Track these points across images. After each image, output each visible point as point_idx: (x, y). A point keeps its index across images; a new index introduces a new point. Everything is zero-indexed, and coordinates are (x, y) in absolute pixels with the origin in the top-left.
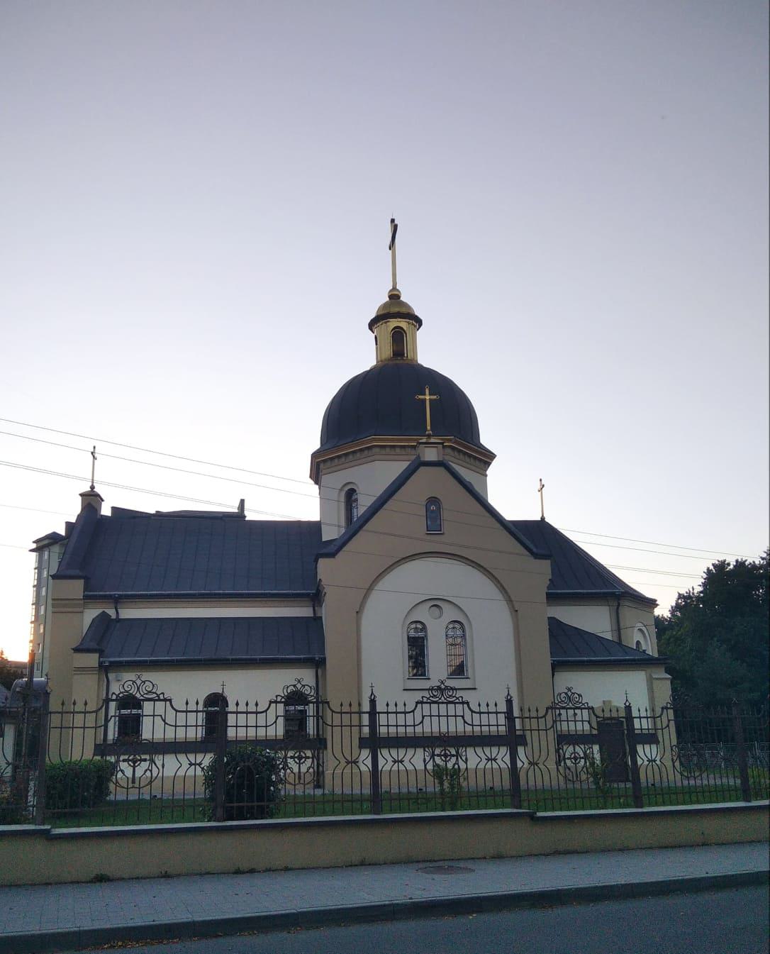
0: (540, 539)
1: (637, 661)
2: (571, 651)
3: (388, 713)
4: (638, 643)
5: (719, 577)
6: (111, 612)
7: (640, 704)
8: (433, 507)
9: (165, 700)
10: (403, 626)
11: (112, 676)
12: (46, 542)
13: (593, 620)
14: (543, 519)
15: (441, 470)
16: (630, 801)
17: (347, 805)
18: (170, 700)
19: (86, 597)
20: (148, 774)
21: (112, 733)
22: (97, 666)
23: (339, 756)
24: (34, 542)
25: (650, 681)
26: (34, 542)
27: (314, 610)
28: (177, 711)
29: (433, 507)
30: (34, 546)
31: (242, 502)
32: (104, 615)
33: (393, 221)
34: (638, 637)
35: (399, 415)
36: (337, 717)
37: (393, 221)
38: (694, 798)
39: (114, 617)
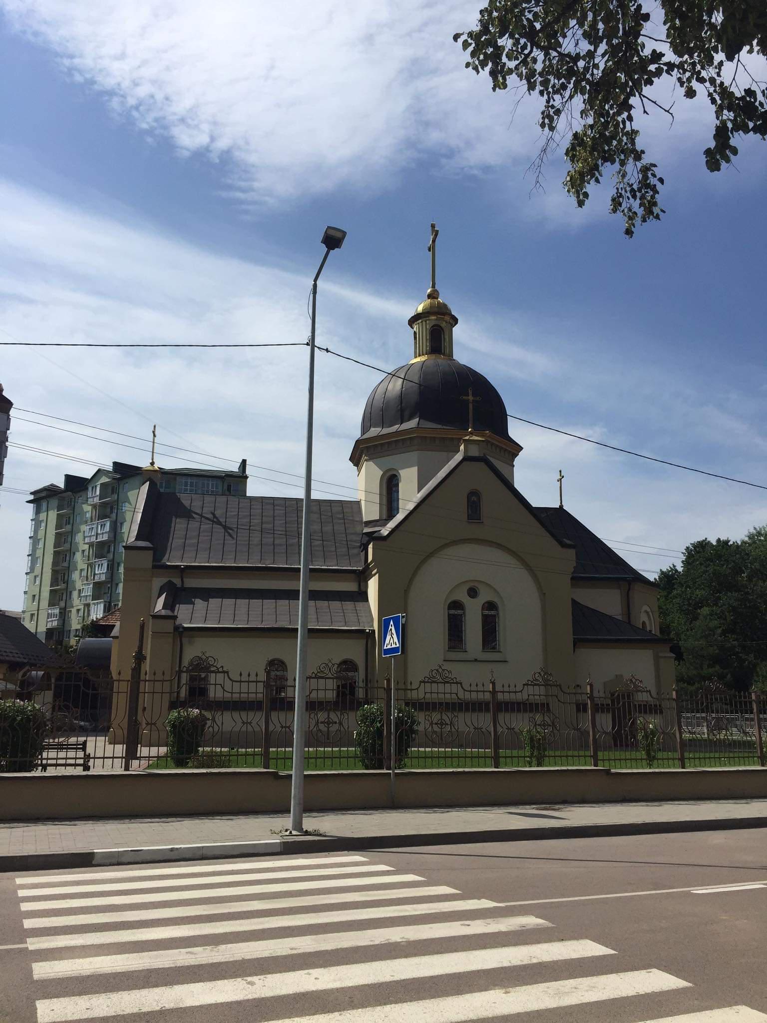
0: (559, 524)
1: (636, 638)
2: (589, 629)
3: (503, 692)
4: (644, 623)
5: (700, 553)
6: (177, 581)
7: (647, 679)
8: (474, 498)
9: (224, 672)
10: (445, 601)
11: (185, 640)
12: (43, 494)
13: (606, 601)
14: (561, 507)
15: (482, 465)
16: (534, 761)
17: (422, 761)
18: (227, 672)
19: (154, 567)
20: (211, 729)
21: (183, 693)
22: (172, 631)
23: (503, 725)
24: (31, 493)
25: (657, 659)
26: (31, 493)
27: (360, 585)
28: (233, 681)
29: (474, 498)
30: (32, 497)
31: (244, 462)
32: (170, 583)
33: (433, 226)
34: (644, 618)
35: (445, 410)
36: (236, 685)
37: (433, 226)
38: (629, 765)
39: (179, 585)
